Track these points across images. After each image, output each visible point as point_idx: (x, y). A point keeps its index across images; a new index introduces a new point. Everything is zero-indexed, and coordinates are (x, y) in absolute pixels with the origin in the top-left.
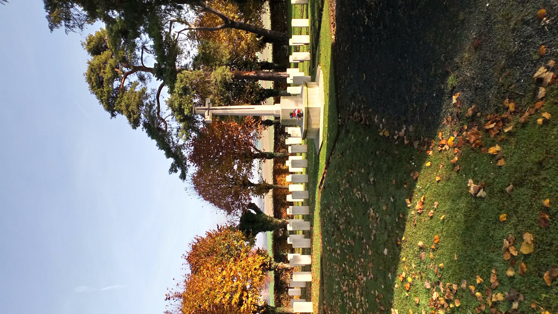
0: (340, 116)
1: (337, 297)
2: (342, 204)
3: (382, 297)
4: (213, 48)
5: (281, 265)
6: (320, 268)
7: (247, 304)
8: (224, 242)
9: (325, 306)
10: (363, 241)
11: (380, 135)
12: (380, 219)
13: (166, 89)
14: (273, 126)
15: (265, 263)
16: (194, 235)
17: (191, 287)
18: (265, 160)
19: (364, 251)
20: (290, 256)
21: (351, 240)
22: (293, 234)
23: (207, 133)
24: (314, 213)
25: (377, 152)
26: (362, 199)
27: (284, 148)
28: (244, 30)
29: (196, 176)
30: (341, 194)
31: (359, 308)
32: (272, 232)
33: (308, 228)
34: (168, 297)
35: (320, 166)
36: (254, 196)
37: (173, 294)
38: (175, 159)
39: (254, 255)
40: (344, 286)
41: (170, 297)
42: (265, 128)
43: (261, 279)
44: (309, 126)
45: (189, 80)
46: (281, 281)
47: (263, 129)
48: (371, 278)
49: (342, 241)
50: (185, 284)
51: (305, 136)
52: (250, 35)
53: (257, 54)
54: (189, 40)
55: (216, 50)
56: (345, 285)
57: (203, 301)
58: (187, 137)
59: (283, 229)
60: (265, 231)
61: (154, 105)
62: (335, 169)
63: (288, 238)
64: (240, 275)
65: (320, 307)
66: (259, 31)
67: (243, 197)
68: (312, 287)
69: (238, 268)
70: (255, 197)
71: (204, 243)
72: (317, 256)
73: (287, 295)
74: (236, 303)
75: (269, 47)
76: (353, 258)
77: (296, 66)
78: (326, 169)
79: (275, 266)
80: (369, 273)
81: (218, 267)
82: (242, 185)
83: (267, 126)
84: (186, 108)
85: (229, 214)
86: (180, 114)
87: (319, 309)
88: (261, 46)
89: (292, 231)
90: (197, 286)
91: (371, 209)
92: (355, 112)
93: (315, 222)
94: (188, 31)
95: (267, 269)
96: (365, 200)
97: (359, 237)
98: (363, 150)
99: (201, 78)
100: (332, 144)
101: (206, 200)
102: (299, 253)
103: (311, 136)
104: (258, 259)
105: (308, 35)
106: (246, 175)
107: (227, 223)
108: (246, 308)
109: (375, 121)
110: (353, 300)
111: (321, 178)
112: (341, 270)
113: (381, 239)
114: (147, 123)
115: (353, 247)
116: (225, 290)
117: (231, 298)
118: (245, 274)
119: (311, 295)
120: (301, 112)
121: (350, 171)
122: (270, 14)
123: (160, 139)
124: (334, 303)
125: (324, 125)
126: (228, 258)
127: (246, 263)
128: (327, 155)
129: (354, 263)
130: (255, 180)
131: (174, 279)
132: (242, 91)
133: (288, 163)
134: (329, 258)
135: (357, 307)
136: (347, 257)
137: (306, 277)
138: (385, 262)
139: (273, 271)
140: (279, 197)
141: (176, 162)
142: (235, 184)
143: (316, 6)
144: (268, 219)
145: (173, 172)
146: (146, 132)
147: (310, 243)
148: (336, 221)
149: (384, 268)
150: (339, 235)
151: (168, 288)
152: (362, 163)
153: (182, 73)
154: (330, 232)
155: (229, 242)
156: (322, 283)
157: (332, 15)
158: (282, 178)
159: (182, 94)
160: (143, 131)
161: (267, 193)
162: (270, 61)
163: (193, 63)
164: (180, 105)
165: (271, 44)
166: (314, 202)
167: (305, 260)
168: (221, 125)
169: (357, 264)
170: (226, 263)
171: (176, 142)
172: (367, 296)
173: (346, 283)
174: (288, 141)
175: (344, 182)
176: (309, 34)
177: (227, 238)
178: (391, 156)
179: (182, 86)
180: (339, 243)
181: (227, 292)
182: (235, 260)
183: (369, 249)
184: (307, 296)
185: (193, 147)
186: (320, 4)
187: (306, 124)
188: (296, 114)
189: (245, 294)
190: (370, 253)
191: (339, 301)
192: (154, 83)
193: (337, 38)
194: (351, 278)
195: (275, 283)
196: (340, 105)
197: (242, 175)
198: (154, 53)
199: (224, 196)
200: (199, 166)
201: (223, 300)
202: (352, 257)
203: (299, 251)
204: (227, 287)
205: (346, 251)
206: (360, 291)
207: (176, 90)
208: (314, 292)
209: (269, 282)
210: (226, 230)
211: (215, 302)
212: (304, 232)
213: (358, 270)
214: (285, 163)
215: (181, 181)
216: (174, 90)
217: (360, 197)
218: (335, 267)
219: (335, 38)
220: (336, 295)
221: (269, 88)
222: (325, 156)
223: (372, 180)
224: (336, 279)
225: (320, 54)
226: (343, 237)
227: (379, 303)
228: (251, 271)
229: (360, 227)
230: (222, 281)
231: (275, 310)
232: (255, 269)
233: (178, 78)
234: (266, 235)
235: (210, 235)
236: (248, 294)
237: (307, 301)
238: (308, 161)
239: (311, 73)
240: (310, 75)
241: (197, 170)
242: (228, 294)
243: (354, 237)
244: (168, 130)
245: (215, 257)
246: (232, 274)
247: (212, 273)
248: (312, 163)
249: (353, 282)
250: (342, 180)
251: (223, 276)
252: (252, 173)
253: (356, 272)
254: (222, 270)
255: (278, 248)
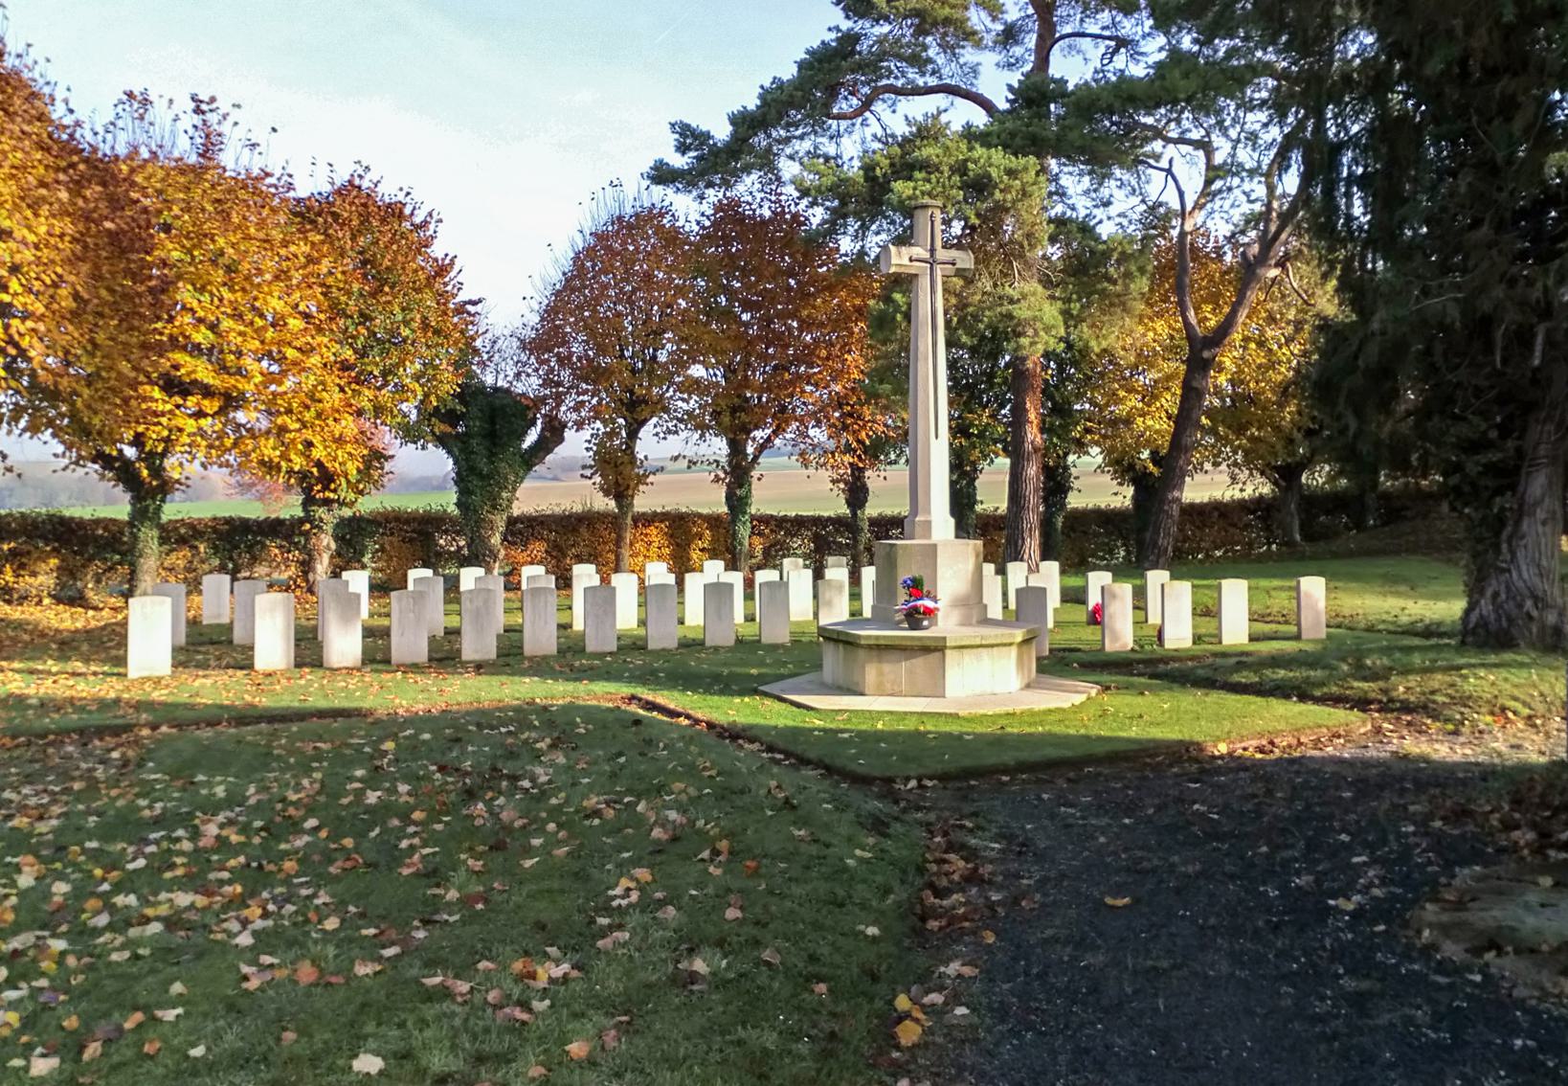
0: (930, 784)
1: (176, 795)
2: (577, 812)
3: (147, 1048)
4: (1126, 291)
5: (325, 543)
6: (307, 705)
7: (171, 412)
8: (415, 325)
9: (146, 732)
10: (416, 923)
11: (895, 997)
12: (524, 1023)
13: (980, 118)
14: (844, 510)
15: (334, 481)
16: (443, 210)
17: (242, 194)
18: (723, 480)
19: (372, 931)
20: (358, 580)
21: (424, 857)
22: (447, 591)
23: (820, 266)
24: (530, 675)
25: (822, 988)
26: (607, 910)
27: (766, 552)
28: (1181, 409)
29: (665, 221)
30: (619, 802)
31: (111, 908)
32: (453, 509)
33: (470, 651)
34: (204, 107)
35: (716, 698)
36: (589, 442)
37: (216, 127)
38: (727, 145)
39: (363, 435)
40: (222, 826)
41: (203, 113)
42: (838, 481)
43: (270, 467)
44: (874, 653)
45: (1014, 202)
46: (264, 546)
47: (835, 476)
48: (246, 978)
49: (417, 815)
50: (256, 172)
51: (834, 637)
52: (1165, 426)
53: (1095, 456)
54: (1143, 207)
55: (1117, 303)
56: (224, 833)
57: (187, 237)
58: (809, 189)
59: (465, 552)
60: (456, 483)
61: (923, 74)
62: (718, 774)
63: (428, 573)
64: (289, 383)
65: (146, 711)
66: (1172, 462)
67: (586, 398)
68: (230, 672)
69: (312, 378)
70: (587, 445)
71: (410, 248)
72: (355, 691)
73: (206, 567)
74: (176, 367)
75: (1120, 497)
76: (344, 870)
77: (1074, 596)
78: (711, 725)
79: (321, 520)
80: (271, 966)
81: (318, 301)
82: (632, 393)
83: (843, 491)
84: (915, 189)
85: (524, 345)
86: (892, 165)
87: (139, 706)
88: (1123, 467)
89: (458, 587)
90: (245, 218)
91: (565, 967)
92: (967, 861)
93: (495, 680)
94: (1176, 205)
95: (310, 488)
96: (604, 932)
97: (436, 904)
98: (818, 911)
99: (1022, 247)
100: (812, 755)
101: (577, 258)
102: (371, 615)
103: (832, 659)
104: (350, 454)
105: (1194, 643)
106: (666, 410)
107: (489, 336)
108: (153, 405)
109: (947, 963)
110: (150, 882)
111: (672, 706)
112: (291, 811)
113: (428, 1033)
114: (854, 48)
115: (390, 869)
116: (227, 324)
117: (196, 350)
118: (290, 404)
119: (199, 666)
120: (925, 623)
121: (723, 845)
122: (1227, 497)
123: (800, 93)
124: (153, 777)
125: (881, 714)
126: (353, 337)
127: (332, 408)
128: (767, 729)
129: (320, 880)
130: (650, 445)
131: (274, 130)
132: (972, 397)
133: (714, 570)
134: (348, 752)
135: (120, 900)
136: (349, 842)
137: (272, 647)
138: (314, 1060)
139: (302, 515)
140: (586, 535)
141: (715, 151)
142: (634, 371)
143: (1312, 673)
144: (504, 495)
145: (677, 136)
146: (823, 42)
147: (409, 660)
148: (504, 783)
149: (285, 1055)
150: (444, 798)
151: (239, 106)
152: (765, 907)
153: (1037, 174)
154: (454, 754)
155: (414, 342)
156: (244, 717)
157: (1300, 744)
158: (656, 544)
159: (965, 174)
160: (830, 29)
161: (602, 489)
162: (1074, 501)
163: (1070, 220)
164: (926, 166)
165: (1128, 503)
166: (578, 674)
167: (344, 645)
168: (848, 319)
169: (315, 895)
170: (332, 330)
171: (788, 151)
172: (165, 953)
173: (234, 838)
174: (797, 575)
175: (673, 815)
176: (1197, 647)
177: (430, 334)
178: (819, 1071)
179: (994, 175)
180: (411, 800)
181: (218, 334)
182: (345, 366)
183: (380, 959)
184: (199, 652)
185: (767, 214)
186: (1325, 690)
187: (882, 642)
188: (920, 603)
189: (211, 406)
190: (363, 969)
191: (159, 805)
192: (998, 83)
193: (1220, 762)
194: (254, 864)
195: (255, 521)
196: (973, 783)
197: (668, 395)
198: (1095, 81)
199: (592, 333)
200: (702, 236)
201: (188, 319)
202: (349, 865)
203: (380, 615)
204: (241, 334)
205: (373, 834)
206: (193, 916)
207: (980, 151)
208: (209, 682)
209: (261, 498)
210: (462, 332)
211: (180, 284)
212: (453, 633)
213: (288, 900)
214: (711, 558)
215: (646, 166)
216: (977, 146)
217: (615, 903)
218: (305, 782)
219: (1221, 757)
220: (184, 789)
221: (978, 498)
222: (761, 721)
223: (700, 966)
224: (252, 790)
225: (1142, 694)
226: (434, 816)
227: (120, 1029)
228: (299, 430)
229: (480, 906)
230: (262, 316)
231: (148, 523)
232: (309, 445)
233: (1022, 161)
234: (440, 488)
235: (442, 269)
236: (212, 416)
237: (176, 650)
238: (730, 649)
239: (1061, 654)
240: (1051, 650)
241: (687, 229)
242: (211, 336)
243: (433, 874)
244: (834, 123)
245: (356, 287)
246: (291, 353)
247: (296, 277)
248: (725, 664)
249: (238, 874)
250: (682, 809)
251: (283, 318)
252: (676, 432)
253: (279, 890)
254: (307, 316)
255: (392, 534)
